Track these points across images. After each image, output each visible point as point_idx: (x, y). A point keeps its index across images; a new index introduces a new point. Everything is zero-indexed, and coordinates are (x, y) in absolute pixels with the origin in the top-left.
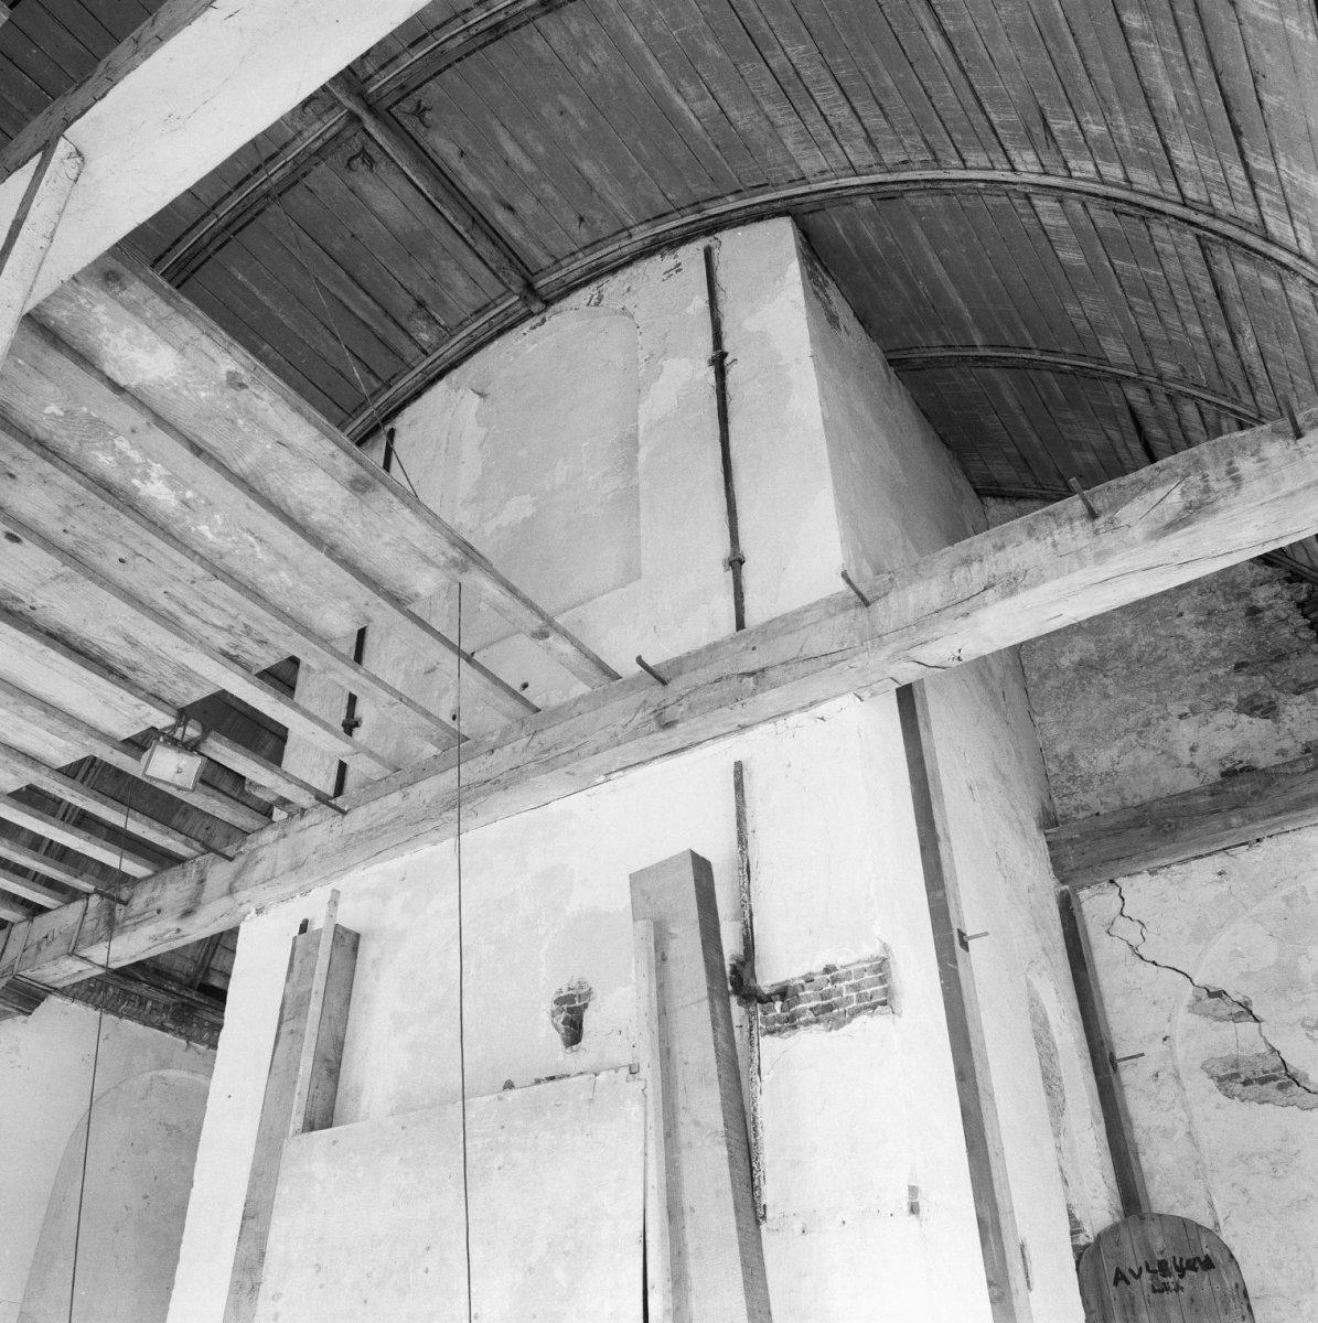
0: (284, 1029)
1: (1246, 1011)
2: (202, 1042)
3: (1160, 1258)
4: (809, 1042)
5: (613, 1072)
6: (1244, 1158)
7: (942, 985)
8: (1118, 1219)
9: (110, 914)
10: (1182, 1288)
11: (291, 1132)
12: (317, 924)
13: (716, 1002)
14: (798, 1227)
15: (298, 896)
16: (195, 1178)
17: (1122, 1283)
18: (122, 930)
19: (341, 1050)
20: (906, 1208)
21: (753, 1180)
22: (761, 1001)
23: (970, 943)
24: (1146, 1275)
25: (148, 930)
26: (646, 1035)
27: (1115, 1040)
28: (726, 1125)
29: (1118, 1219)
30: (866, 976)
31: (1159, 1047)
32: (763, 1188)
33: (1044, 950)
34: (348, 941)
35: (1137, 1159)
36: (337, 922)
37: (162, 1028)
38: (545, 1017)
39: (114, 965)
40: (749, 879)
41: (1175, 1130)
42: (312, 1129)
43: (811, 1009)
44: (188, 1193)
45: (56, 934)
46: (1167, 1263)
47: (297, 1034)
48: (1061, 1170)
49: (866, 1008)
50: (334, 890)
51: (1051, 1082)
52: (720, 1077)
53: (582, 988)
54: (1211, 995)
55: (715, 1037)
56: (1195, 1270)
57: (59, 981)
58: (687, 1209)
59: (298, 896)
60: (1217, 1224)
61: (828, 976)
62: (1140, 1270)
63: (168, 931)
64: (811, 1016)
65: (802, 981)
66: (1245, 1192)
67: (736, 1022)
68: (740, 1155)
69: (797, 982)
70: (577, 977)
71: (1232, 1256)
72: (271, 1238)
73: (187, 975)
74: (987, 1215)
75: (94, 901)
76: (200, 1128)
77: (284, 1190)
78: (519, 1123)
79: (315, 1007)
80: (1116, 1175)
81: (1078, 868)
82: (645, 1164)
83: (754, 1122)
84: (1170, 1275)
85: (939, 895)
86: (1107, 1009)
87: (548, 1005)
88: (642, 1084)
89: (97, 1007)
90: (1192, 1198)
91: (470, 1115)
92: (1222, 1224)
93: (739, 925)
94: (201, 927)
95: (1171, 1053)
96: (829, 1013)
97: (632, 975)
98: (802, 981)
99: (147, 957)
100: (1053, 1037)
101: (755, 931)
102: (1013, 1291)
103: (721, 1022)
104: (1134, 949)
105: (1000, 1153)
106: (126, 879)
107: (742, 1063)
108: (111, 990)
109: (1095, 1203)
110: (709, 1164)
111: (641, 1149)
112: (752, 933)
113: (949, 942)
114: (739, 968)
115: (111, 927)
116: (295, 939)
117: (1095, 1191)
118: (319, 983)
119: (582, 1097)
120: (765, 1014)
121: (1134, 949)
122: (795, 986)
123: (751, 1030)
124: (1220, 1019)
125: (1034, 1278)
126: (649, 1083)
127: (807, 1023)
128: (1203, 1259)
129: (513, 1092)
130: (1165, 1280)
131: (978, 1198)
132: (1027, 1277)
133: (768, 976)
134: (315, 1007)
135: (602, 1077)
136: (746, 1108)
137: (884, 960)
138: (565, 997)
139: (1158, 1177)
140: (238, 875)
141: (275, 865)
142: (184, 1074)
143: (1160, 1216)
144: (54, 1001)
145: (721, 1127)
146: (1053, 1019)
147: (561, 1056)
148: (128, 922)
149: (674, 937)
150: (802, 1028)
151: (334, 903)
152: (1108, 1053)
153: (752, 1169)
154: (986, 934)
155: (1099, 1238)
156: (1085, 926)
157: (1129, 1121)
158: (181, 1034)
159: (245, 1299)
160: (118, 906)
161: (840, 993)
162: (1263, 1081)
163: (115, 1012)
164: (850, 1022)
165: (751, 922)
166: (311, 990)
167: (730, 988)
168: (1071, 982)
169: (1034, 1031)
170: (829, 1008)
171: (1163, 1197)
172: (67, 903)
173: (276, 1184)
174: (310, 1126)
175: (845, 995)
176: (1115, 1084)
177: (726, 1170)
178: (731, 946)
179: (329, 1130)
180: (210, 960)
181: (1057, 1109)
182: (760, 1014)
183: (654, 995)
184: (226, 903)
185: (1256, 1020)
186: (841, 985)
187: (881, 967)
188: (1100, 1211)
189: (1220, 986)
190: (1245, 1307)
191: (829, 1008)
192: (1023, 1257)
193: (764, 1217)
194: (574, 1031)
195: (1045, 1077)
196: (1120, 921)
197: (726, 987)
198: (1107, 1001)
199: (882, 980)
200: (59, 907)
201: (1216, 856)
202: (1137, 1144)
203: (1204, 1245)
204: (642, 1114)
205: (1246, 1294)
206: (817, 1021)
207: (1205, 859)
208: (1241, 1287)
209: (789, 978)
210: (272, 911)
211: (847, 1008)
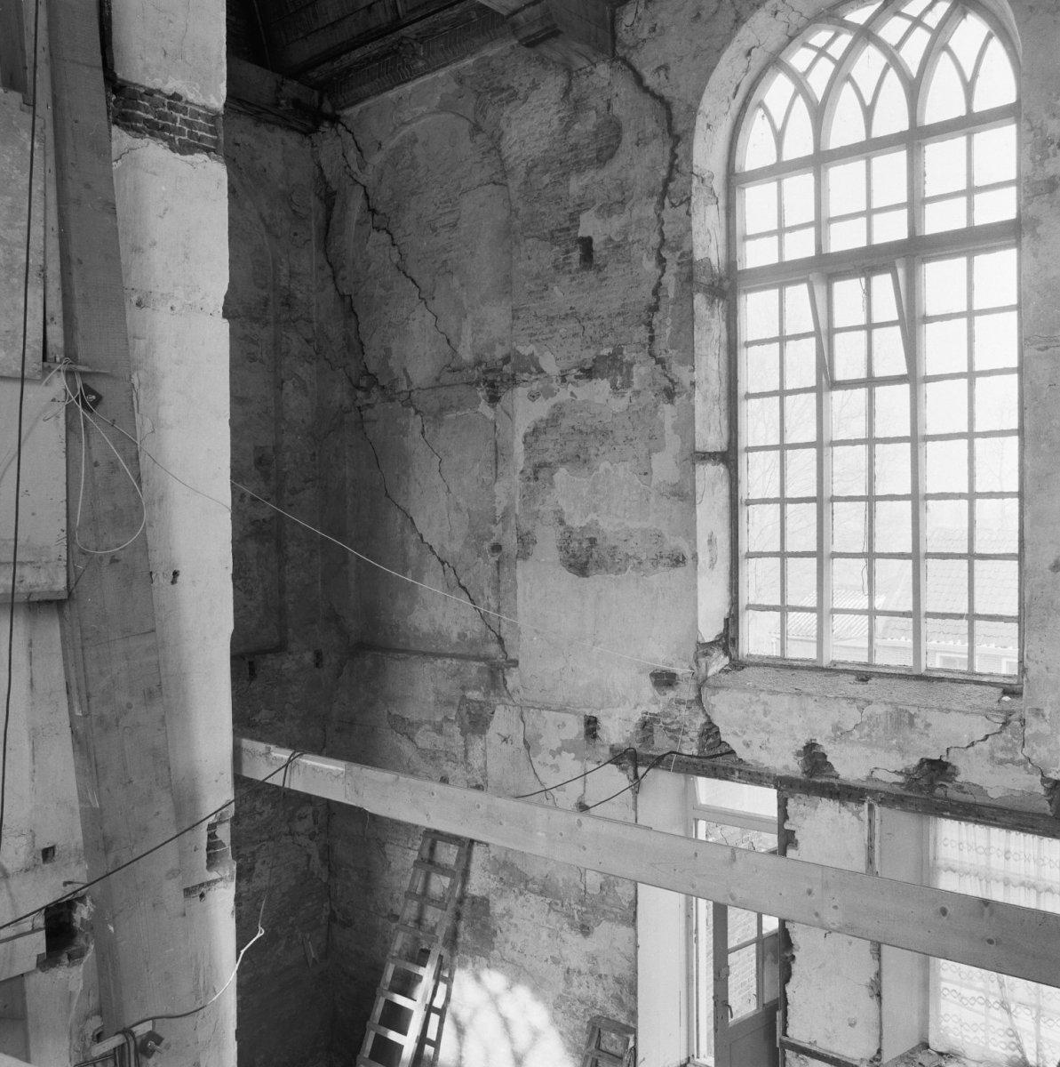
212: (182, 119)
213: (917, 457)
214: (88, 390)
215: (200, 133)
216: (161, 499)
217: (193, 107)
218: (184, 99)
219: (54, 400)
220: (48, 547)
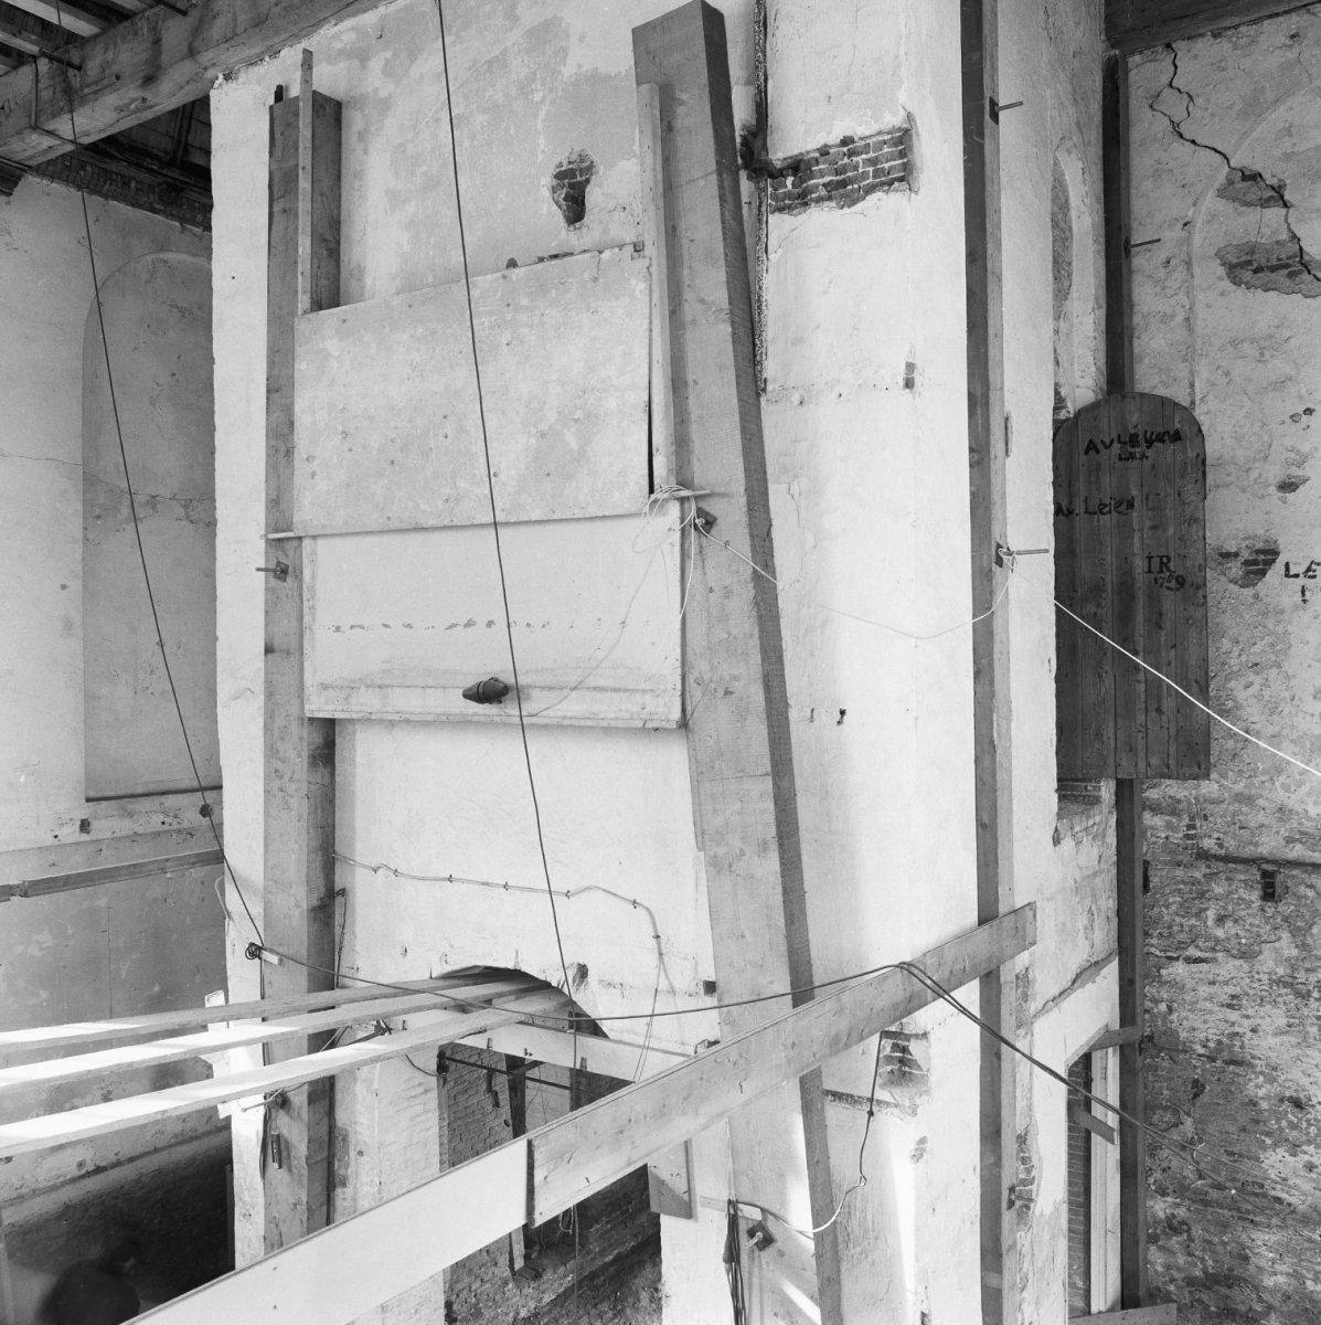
0: (276, 208)
1: (1278, 196)
2: (197, 225)
3: (1132, 431)
4: (820, 220)
5: (617, 250)
6: (1235, 343)
7: (965, 161)
8: (1100, 397)
9: (65, 81)
10: (1147, 457)
11: (300, 312)
12: (295, 91)
13: (725, 175)
14: (796, 398)
15: (267, 59)
16: (215, 356)
17: (1092, 452)
18: (84, 100)
19: (338, 230)
20: (901, 383)
21: (755, 356)
22: (772, 176)
23: (1002, 115)
24: (1116, 446)
25: (111, 100)
26: (652, 208)
27: (1135, 225)
28: (730, 303)
29: (1100, 397)
30: (886, 149)
31: (1177, 233)
32: (765, 363)
33: (1078, 124)
34: (329, 110)
35: (1131, 344)
36: (314, 88)
37: (154, 211)
38: (546, 193)
39: (87, 140)
40: (766, 35)
41: (1173, 316)
42: (321, 308)
43: (824, 185)
44: (211, 372)
45: (12, 104)
46: (1138, 436)
47: (290, 213)
48: (1055, 351)
49: (882, 184)
50: (305, 51)
51: (1061, 267)
52: (726, 255)
53: (582, 161)
54: (1245, 178)
55: (722, 214)
56: (1163, 442)
57: (31, 158)
58: (690, 382)
59: (267, 59)
60: (1193, 403)
61: (845, 149)
62: (1112, 442)
63: (133, 100)
64: (823, 192)
65: (817, 155)
66: (1227, 374)
67: (745, 199)
68: (743, 332)
69: (812, 155)
70: (577, 149)
71: (1200, 431)
72: (297, 410)
73: (166, 152)
74: (979, 392)
75: (43, 64)
76: (211, 309)
77: (302, 366)
78: (524, 301)
79: (304, 184)
80: (1107, 357)
81: (1133, 29)
82: (650, 340)
83: (759, 300)
84: (1138, 446)
85: (975, 57)
86: (1133, 192)
87: (547, 180)
88: (647, 262)
89: (79, 188)
90: (1175, 380)
91: (475, 293)
92: (1197, 403)
93: (752, 90)
94: (168, 96)
95: (1188, 240)
96: (844, 191)
97: (636, 147)
98: (817, 155)
99: (118, 130)
100: (1071, 220)
101: (769, 97)
102: (993, 457)
103: (730, 198)
104: (1175, 125)
105: (999, 335)
106: (72, 38)
107: (749, 241)
108: (89, 168)
109: (1081, 382)
110: (713, 341)
111: (646, 326)
112: (766, 99)
113: (979, 111)
114: (750, 138)
115: (71, 98)
116: (271, 108)
117: (1084, 371)
118: (305, 158)
119: (586, 275)
120: (776, 190)
121: (1175, 125)
122: (809, 160)
123: (760, 206)
124: (1248, 204)
125: (1013, 447)
126: (654, 262)
127: (820, 200)
128: (1172, 432)
129: (517, 270)
130: (1133, 450)
131: (971, 376)
132: (1007, 445)
133: (782, 149)
134: (304, 184)
135: (606, 255)
136: (752, 284)
137: (907, 131)
138: (565, 171)
139: (1147, 361)
140: (196, 33)
141: (235, 20)
142: (184, 257)
143: (1142, 395)
144: (31, 182)
145: (725, 305)
146: (1074, 201)
147: (564, 233)
148: (86, 91)
149: (682, 103)
150: (813, 205)
151: (308, 62)
152: (1124, 238)
153: (754, 345)
154: (1021, 104)
155: (1079, 413)
156: (1128, 98)
157: (1131, 307)
158: (173, 217)
159: (283, 462)
160: (71, 72)
161: (856, 168)
162: (1273, 269)
163: (99, 193)
164: (864, 199)
165: (766, 86)
166: (297, 165)
167: (740, 161)
168: (1100, 162)
169: (1053, 214)
170: (843, 184)
171: (1148, 378)
172: (15, 68)
173: (294, 360)
174: (318, 305)
175: (860, 170)
176: (1125, 271)
177: (730, 347)
178: (742, 112)
179: (338, 309)
180: (187, 137)
181: (1061, 293)
182: (770, 189)
183: (659, 168)
184: (188, 68)
185: (1286, 205)
186: (859, 159)
187: (903, 139)
188: (1084, 386)
189: (1257, 167)
190: (1200, 473)
191: (843, 184)
192: (1006, 428)
193: (764, 390)
194: (575, 208)
195: (1056, 262)
196: (1168, 91)
197: (736, 161)
198: (1134, 183)
199: (902, 154)
200: (6, 73)
201: (1294, 14)
202: (1134, 329)
203: (1177, 420)
204: (647, 292)
205: (1204, 462)
206: (830, 198)
207: (1281, 19)
208: (1201, 457)
209: (804, 150)
210: (242, 77)
211: (861, 185)
212: (864, 161)
213: (533, 1171)
214: (701, 512)
215: (886, 166)
216: (824, 624)
217: (874, 139)
218: (856, 139)
219: (670, 530)
220: (665, 676)
